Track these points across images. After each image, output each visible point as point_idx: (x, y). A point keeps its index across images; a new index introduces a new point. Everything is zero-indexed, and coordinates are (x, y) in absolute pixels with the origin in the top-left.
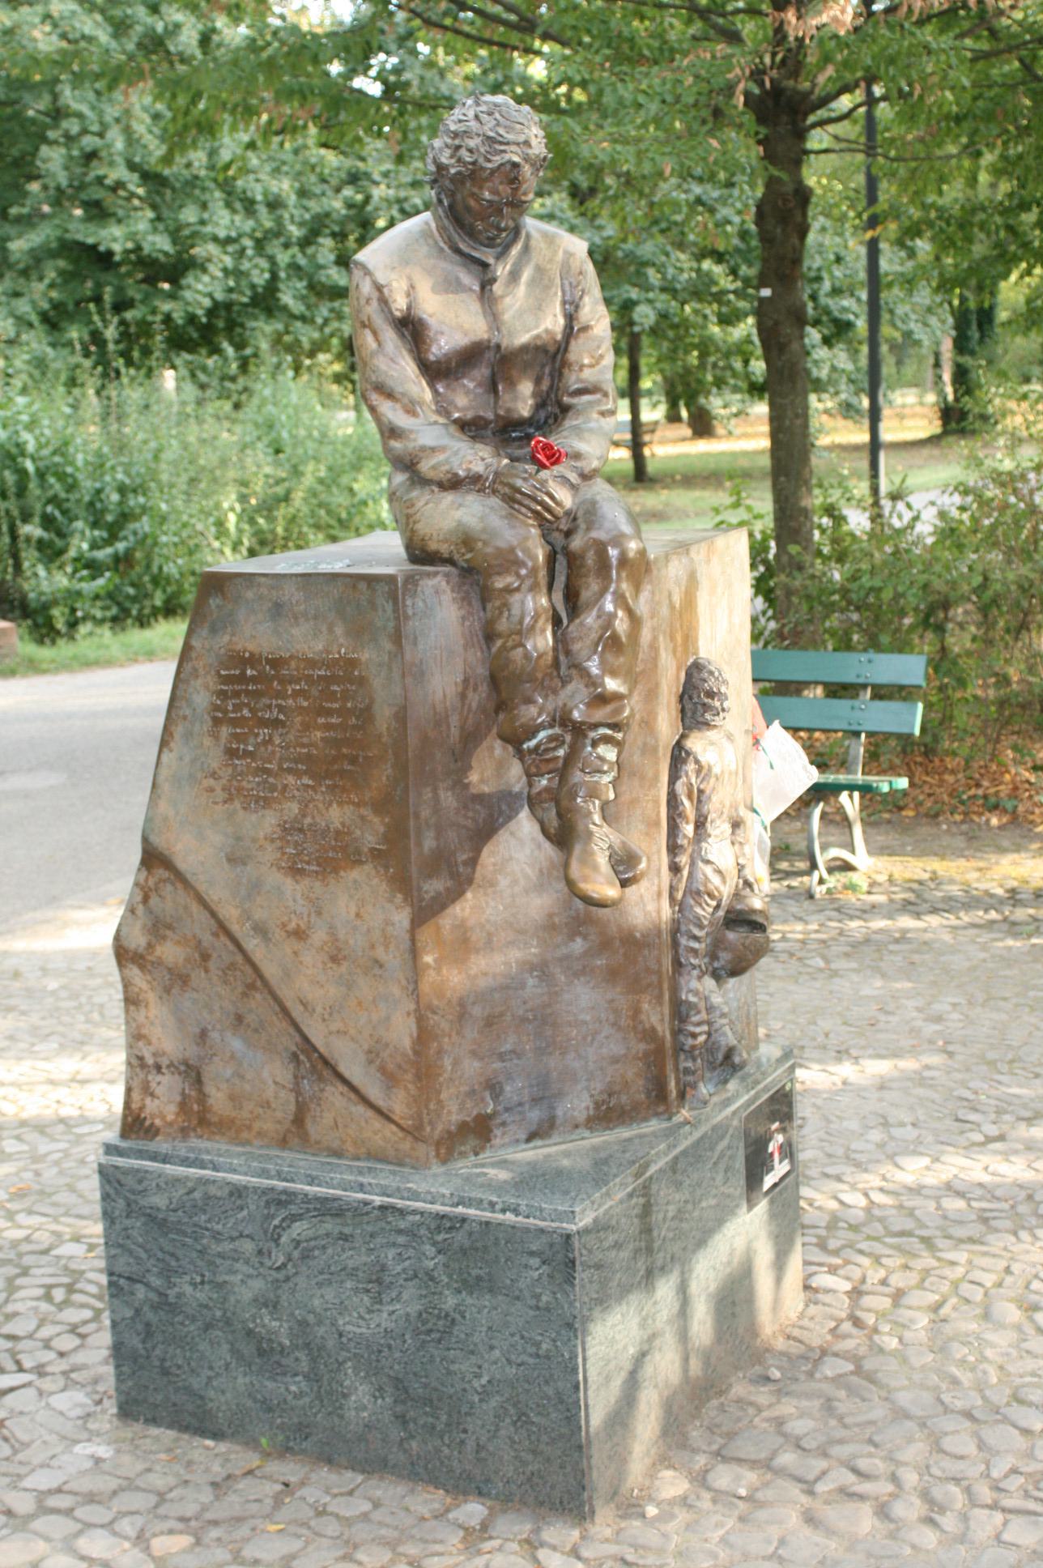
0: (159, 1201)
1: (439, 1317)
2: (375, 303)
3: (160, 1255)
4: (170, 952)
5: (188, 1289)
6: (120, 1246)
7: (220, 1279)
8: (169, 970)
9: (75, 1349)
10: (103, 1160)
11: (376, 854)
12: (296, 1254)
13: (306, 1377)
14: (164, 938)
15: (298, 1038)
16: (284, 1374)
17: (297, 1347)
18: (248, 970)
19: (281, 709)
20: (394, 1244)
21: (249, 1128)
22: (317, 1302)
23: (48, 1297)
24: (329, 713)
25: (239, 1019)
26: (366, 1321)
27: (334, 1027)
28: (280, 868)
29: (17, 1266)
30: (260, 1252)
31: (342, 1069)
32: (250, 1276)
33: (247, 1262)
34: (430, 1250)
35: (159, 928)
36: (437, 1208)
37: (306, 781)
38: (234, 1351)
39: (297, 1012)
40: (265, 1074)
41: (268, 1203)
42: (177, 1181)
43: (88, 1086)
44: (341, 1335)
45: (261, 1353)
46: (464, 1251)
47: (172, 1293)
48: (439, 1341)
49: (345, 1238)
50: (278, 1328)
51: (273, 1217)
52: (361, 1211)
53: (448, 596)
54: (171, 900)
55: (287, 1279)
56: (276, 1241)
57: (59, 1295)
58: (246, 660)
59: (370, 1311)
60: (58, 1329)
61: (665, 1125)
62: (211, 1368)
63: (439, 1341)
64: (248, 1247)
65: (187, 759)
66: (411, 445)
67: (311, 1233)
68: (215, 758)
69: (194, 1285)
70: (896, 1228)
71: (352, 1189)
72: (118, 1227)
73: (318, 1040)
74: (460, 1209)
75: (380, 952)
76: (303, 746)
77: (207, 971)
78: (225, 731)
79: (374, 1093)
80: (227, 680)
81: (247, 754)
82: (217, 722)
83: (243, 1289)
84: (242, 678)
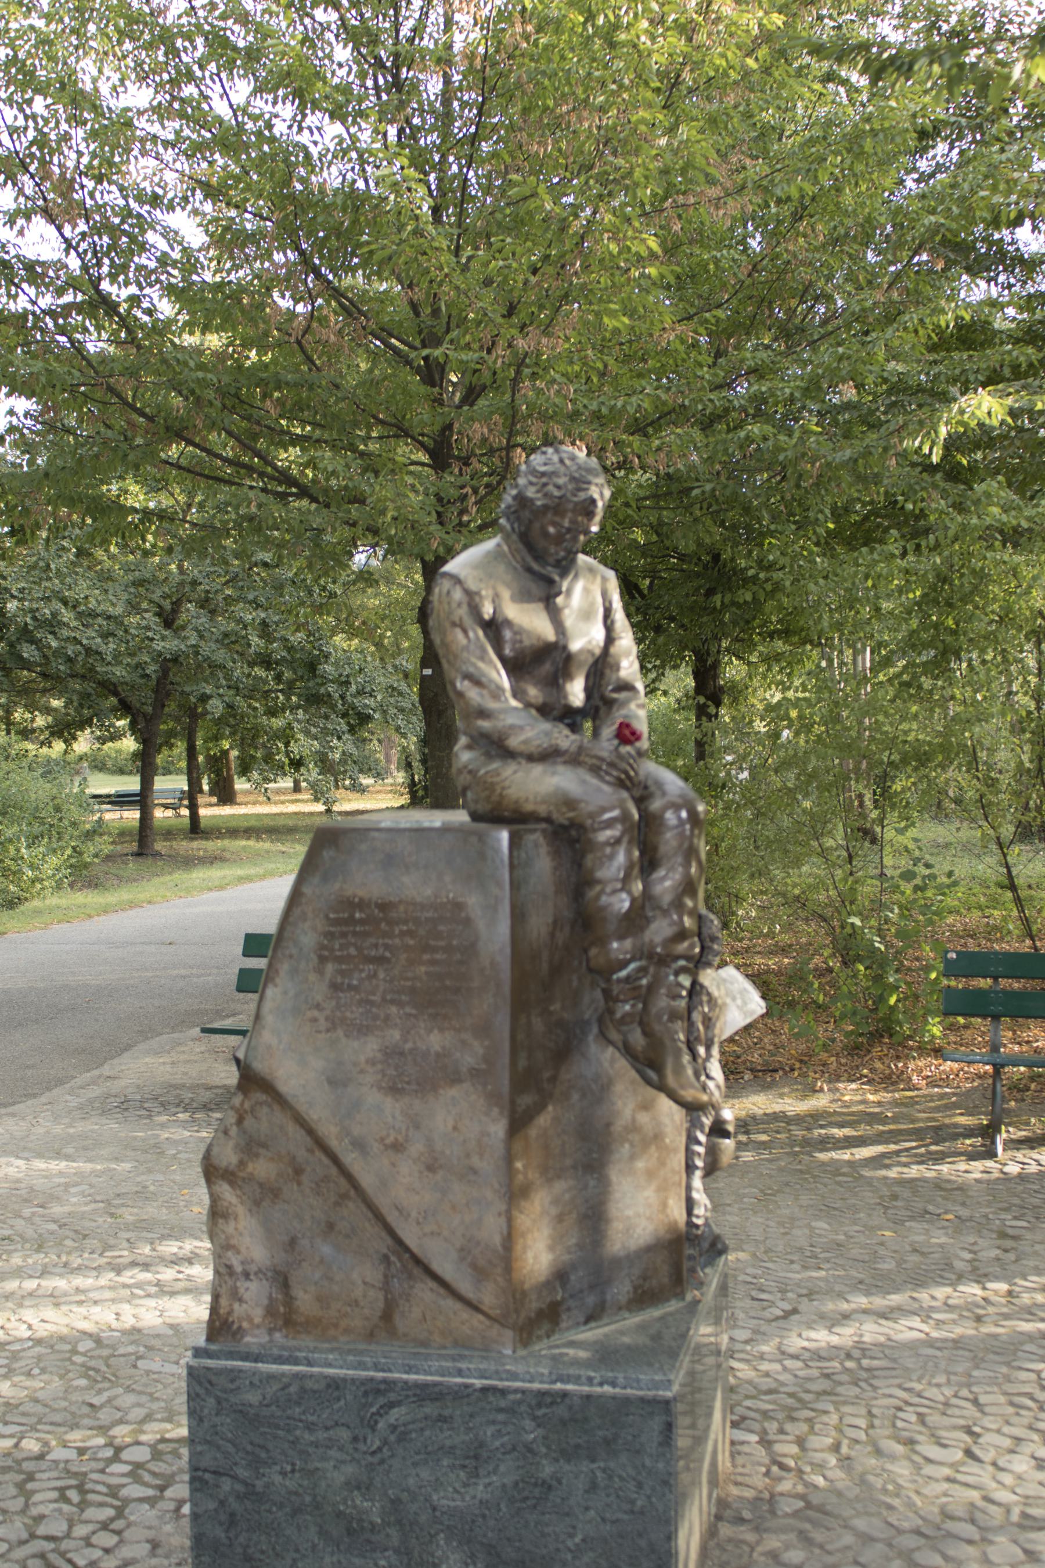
0: (253, 1398)
1: (536, 1485)
2: (465, 607)
3: (249, 1448)
4: (262, 1168)
5: (278, 1479)
6: (207, 1442)
7: (311, 1466)
8: (261, 1185)
9: (117, 1545)
10: (194, 1362)
11: (475, 1074)
12: (392, 1438)
13: (397, 1551)
14: (257, 1155)
15: (389, 1241)
16: (374, 1550)
17: (389, 1524)
18: (343, 1181)
19: (387, 947)
20: (494, 1422)
21: (336, 1326)
22: (411, 1481)
23: (64, 1498)
24: (434, 950)
25: (331, 1226)
26: (457, 1494)
27: (427, 1229)
28: (380, 1088)
29: (20, 1472)
30: (355, 1439)
31: (436, 1266)
32: (343, 1462)
33: (341, 1449)
34: (528, 1424)
35: (251, 1147)
36: (536, 1386)
37: (408, 1010)
38: (322, 1533)
39: (392, 1218)
40: (355, 1276)
41: (366, 1394)
42: (271, 1377)
43: (163, 1297)
44: (434, 1509)
45: (350, 1532)
46: (564, 1423)
47: (259, 1484)
48: (535, 1507)
49: (442, 1419)
50: (373, 1509)
51: (371, 1405)
52: (462, 1394)
53: (544, 850)
54: (267, 1120)
55: (382, 1462)
56: (373, 1429)
57: (73, 1495)
58: (351, 904)
59: (465, 1485)
60: (90, 1528)
61: (681, 1304)
62: (297, 1551)
63: (535, 1507)
64: (344, 1434)
65: (291, 993)
66: (500, 724)
67: (408, 1418)
68: (320, 991)
69: (283, 1474)
70: (765, 1388)
71: (450, 1375)
72: (206, 1424)
73: (411, 1240)
74: (559, 1386)
75: (475, 1161)
76: (407, 979)
77: (299, 1184)
78: (330, 968)
79: (465, 1286)
80: (337, 922)
81: (351, 988)
82: (322, 959)
83: (336, 1474)
84: (351, 921)
